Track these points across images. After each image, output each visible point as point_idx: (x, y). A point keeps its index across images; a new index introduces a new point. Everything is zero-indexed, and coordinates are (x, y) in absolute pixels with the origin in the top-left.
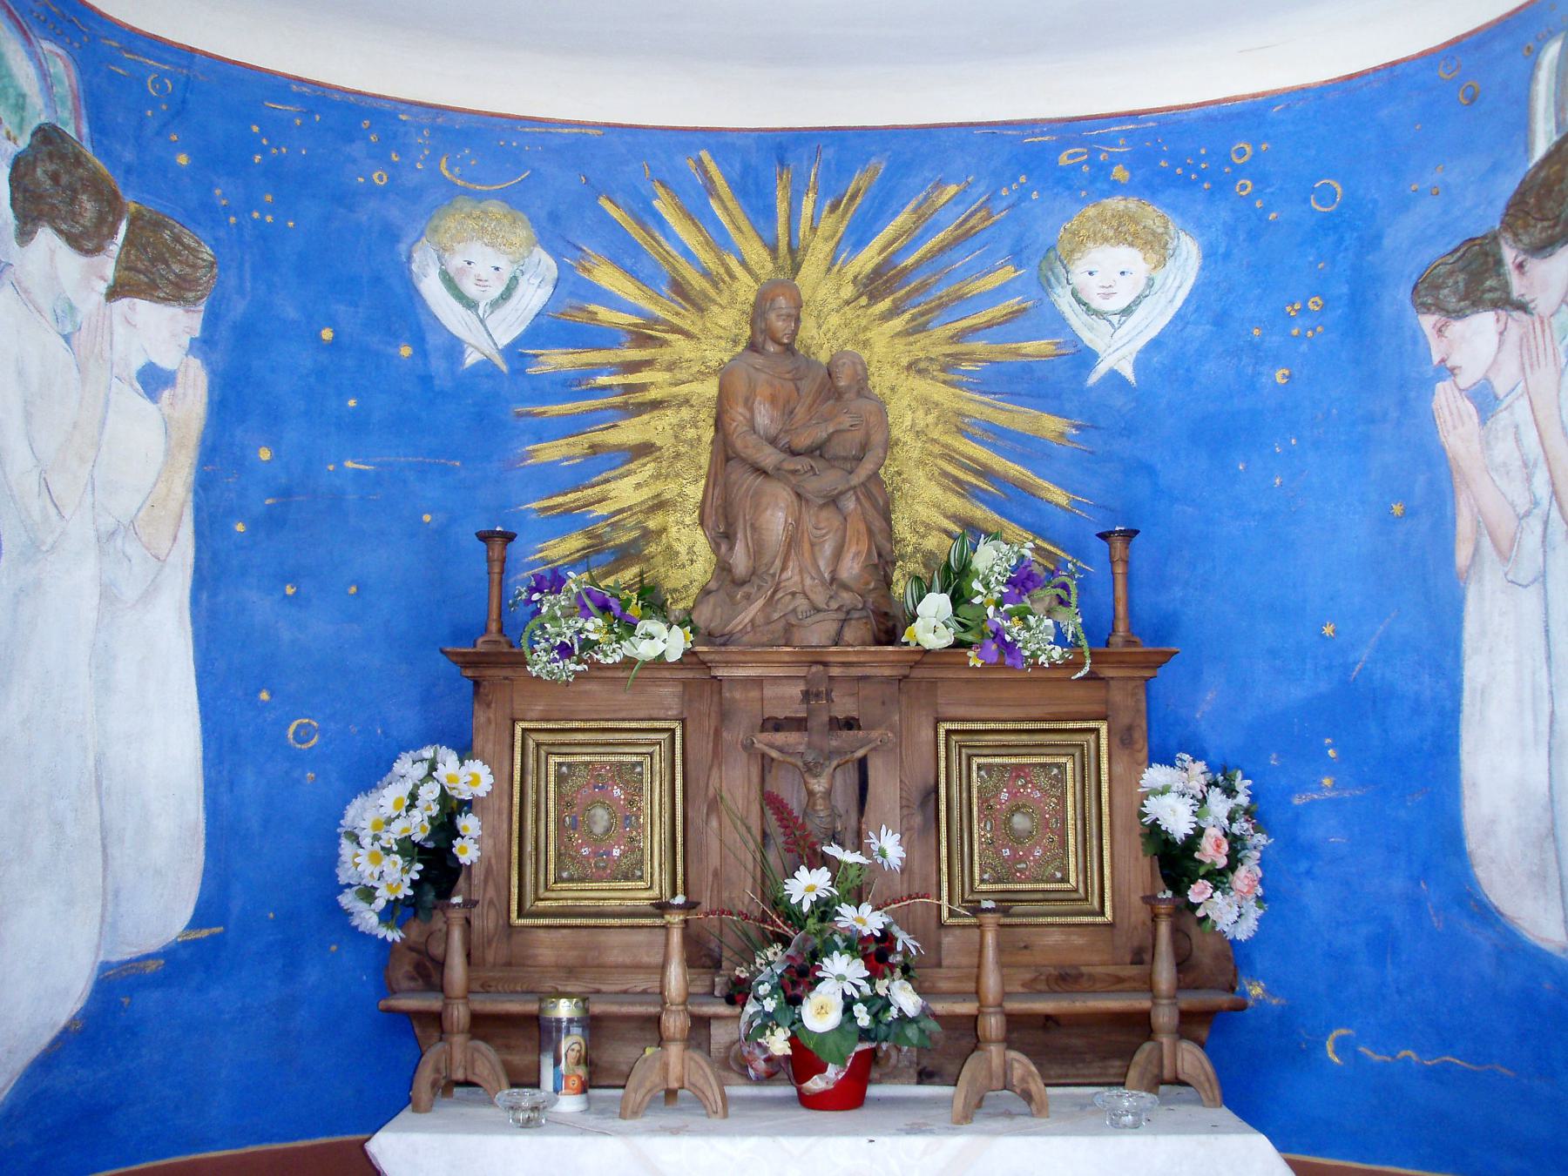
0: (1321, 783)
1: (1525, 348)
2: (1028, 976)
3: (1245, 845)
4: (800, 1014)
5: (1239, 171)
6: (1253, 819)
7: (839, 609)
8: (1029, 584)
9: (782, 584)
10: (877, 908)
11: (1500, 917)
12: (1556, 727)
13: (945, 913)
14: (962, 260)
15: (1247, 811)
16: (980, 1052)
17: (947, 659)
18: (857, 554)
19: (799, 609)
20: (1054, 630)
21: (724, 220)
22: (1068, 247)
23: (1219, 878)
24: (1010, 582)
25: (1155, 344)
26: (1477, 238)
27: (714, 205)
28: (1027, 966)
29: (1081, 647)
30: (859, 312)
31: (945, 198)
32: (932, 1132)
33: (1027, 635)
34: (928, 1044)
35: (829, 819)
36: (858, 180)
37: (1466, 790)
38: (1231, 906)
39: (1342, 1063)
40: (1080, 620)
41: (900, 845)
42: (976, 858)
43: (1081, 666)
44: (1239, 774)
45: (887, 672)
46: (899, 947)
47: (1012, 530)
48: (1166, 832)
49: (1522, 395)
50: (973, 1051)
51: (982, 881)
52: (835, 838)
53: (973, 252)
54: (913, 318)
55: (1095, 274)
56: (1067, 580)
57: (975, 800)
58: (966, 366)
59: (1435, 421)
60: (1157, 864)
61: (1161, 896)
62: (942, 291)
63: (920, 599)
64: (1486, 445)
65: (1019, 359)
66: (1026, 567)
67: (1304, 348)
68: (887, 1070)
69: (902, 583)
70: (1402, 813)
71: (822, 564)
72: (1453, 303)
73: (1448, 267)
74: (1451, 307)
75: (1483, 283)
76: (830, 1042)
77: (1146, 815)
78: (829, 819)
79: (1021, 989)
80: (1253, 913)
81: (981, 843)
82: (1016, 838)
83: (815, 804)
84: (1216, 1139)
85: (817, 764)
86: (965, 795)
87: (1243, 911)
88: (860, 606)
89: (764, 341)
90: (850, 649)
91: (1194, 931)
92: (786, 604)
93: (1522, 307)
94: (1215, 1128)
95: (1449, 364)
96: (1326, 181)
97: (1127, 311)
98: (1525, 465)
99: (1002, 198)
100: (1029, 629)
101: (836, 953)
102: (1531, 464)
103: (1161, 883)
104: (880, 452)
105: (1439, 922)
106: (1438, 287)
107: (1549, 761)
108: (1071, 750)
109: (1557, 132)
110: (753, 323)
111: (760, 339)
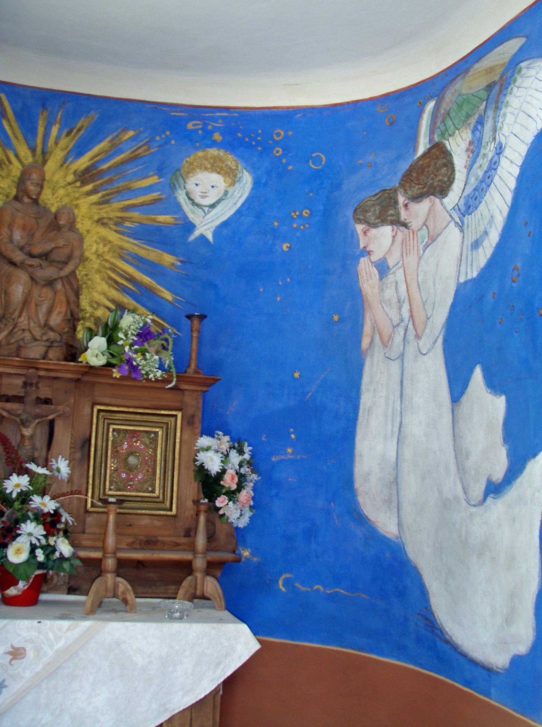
0: (286, 451)
1: (404, 245)
2: (130, 540)
3: (246, 479)
4: (6, 553)
5: (276, 143)
6: (251, 466)
7: (47, 340)
8: (148, 337)
9: (19, 324)
10: (53, 498)
11: (368, 521)
12: (402, 429)
13: (89, 505)
14: (132, 170)
15: (249, 463)
16: (102, 577)
17: (101, 372)
18: (60, 313)
19: (26, 339)
20: (158, 363)
21: (9, 132)
22: (187, 170)
23: (232, 495)
24: (139, 335)
25: (225, 224)
26: (387, 190)
27: (5, 123)
28: (129, 535)
29: (172, 372)
30: (75, 190)
31: (126, 137)
32: (72, 618)
33: (145, 363)
34: (74, 573)
35: (31, 451)
36: (83, 122)
37: (357, 459)
38: (236, 510)
39: (286, 591)
40: (173, 359)
41: (68, 466)
42: (108, 477)
43: (170, 382)
44: (246, 444)
45: (69, 376)
46: (63, 520)
47: (142, 309)
48: (207, 470)
49: (401, 267)
50: (97, 577)
51: (110, 490)
52: (34, 460)
53: (138, 166)
54: (103, 196)
55: (199, 186)
56: (168, 337)
57: (110, 447)
58: (128, 224)
59: (358, 276)
60: (201, 487)
61: (202, 501)
62: (121, 184)
63: (90, 339)
64: (382, 290)
65: (155, 224)
66: (148, 328)
67: (298, 234)
68: (51, 586)
69: (82, 332)
70: (325, 468)
71: (41, 316)
72: (372, 219)
73: (372, 202)
74: (371, 222)
75: (388, 212)
76: (21, 570)
77: (197, 461)
78: (31, 451)
79: (126, 547)
80: (248, 514)
81: (111, 470)
82: (130, 469)
83: (24, 442)
84: (222, 626)
85: (27, 421)
86: (104, 444)
87: (243, 512)
88: (59, 340)
89: (23, 196)
90: (51, 362)
91: (217, 521)
92: (19, 335)
93: (405, 225)
94: (221, 621)
95: (368, 249)
96: (318, 154)
97: (213, 206)
98: (399, 301)
99: (156, 141)
100: (146, 360)
101: (29, 521)
102: (401, 301)
103: (202, 496)
104: (77, 260)
105: (338, 523)
106: (366, 211)
107: (398, 446)
108: (161, 425)
109: (429, 143)
110: (18, 188)
111: (20, 194)
